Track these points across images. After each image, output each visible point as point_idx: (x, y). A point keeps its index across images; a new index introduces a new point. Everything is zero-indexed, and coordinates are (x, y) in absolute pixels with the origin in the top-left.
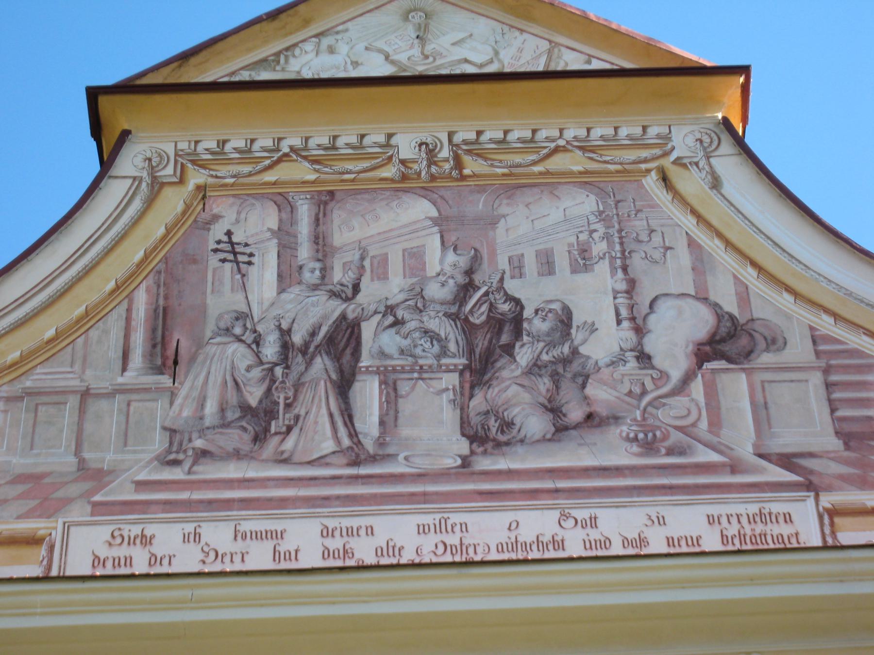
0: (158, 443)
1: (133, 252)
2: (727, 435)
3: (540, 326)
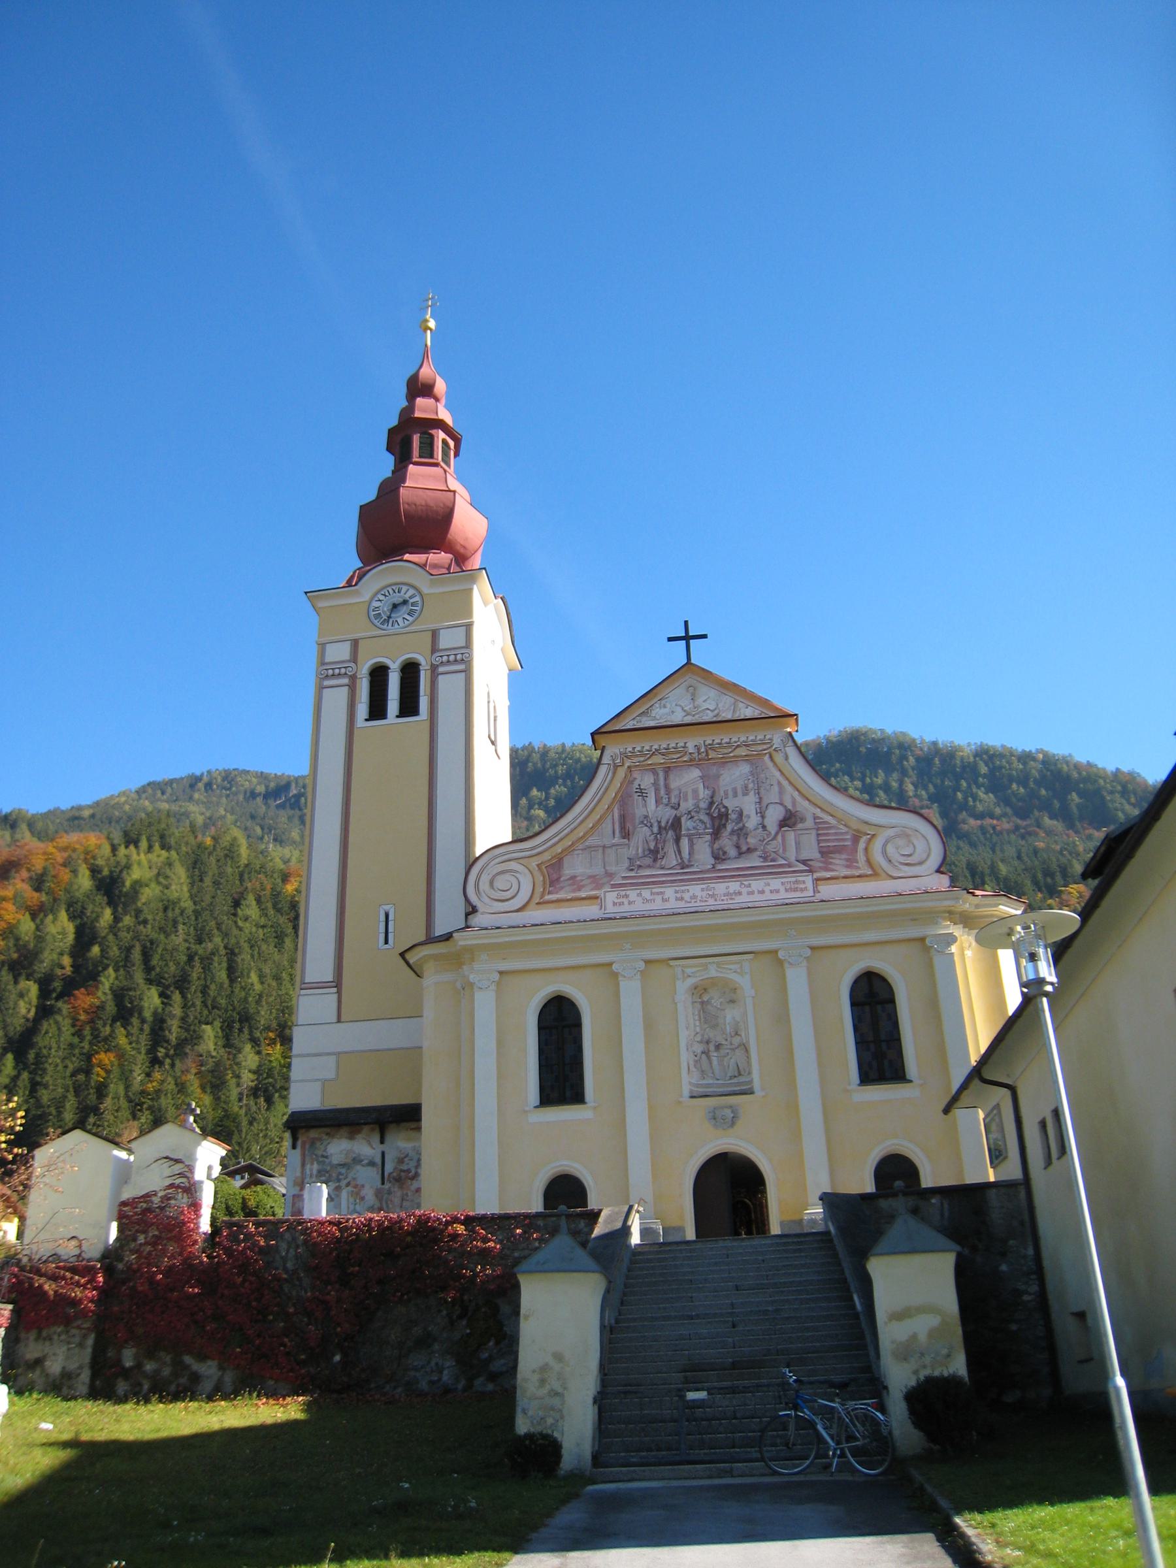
0: (626, 864)
1: (612, 794)
2: (788, 854)
3: (733, 816)
